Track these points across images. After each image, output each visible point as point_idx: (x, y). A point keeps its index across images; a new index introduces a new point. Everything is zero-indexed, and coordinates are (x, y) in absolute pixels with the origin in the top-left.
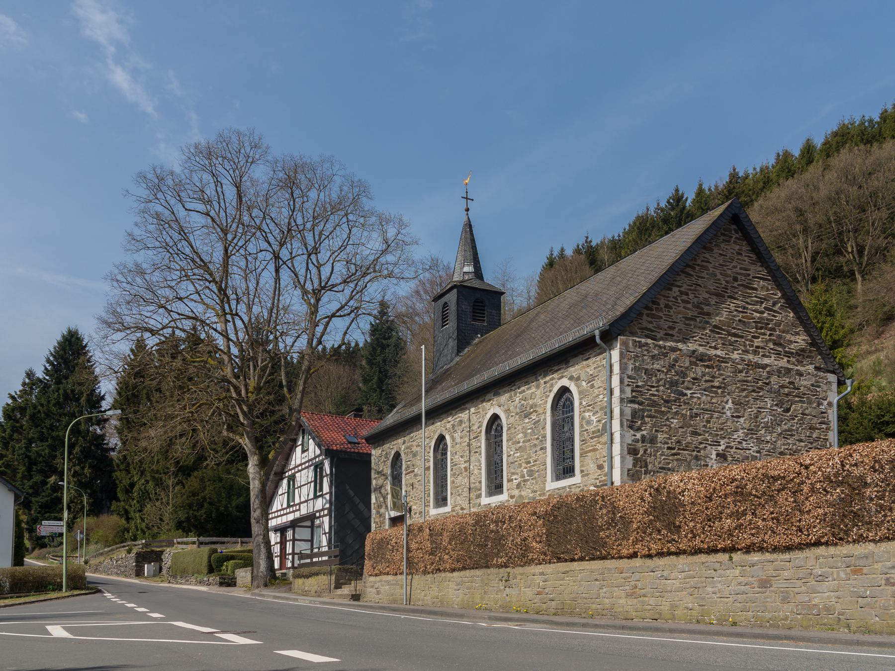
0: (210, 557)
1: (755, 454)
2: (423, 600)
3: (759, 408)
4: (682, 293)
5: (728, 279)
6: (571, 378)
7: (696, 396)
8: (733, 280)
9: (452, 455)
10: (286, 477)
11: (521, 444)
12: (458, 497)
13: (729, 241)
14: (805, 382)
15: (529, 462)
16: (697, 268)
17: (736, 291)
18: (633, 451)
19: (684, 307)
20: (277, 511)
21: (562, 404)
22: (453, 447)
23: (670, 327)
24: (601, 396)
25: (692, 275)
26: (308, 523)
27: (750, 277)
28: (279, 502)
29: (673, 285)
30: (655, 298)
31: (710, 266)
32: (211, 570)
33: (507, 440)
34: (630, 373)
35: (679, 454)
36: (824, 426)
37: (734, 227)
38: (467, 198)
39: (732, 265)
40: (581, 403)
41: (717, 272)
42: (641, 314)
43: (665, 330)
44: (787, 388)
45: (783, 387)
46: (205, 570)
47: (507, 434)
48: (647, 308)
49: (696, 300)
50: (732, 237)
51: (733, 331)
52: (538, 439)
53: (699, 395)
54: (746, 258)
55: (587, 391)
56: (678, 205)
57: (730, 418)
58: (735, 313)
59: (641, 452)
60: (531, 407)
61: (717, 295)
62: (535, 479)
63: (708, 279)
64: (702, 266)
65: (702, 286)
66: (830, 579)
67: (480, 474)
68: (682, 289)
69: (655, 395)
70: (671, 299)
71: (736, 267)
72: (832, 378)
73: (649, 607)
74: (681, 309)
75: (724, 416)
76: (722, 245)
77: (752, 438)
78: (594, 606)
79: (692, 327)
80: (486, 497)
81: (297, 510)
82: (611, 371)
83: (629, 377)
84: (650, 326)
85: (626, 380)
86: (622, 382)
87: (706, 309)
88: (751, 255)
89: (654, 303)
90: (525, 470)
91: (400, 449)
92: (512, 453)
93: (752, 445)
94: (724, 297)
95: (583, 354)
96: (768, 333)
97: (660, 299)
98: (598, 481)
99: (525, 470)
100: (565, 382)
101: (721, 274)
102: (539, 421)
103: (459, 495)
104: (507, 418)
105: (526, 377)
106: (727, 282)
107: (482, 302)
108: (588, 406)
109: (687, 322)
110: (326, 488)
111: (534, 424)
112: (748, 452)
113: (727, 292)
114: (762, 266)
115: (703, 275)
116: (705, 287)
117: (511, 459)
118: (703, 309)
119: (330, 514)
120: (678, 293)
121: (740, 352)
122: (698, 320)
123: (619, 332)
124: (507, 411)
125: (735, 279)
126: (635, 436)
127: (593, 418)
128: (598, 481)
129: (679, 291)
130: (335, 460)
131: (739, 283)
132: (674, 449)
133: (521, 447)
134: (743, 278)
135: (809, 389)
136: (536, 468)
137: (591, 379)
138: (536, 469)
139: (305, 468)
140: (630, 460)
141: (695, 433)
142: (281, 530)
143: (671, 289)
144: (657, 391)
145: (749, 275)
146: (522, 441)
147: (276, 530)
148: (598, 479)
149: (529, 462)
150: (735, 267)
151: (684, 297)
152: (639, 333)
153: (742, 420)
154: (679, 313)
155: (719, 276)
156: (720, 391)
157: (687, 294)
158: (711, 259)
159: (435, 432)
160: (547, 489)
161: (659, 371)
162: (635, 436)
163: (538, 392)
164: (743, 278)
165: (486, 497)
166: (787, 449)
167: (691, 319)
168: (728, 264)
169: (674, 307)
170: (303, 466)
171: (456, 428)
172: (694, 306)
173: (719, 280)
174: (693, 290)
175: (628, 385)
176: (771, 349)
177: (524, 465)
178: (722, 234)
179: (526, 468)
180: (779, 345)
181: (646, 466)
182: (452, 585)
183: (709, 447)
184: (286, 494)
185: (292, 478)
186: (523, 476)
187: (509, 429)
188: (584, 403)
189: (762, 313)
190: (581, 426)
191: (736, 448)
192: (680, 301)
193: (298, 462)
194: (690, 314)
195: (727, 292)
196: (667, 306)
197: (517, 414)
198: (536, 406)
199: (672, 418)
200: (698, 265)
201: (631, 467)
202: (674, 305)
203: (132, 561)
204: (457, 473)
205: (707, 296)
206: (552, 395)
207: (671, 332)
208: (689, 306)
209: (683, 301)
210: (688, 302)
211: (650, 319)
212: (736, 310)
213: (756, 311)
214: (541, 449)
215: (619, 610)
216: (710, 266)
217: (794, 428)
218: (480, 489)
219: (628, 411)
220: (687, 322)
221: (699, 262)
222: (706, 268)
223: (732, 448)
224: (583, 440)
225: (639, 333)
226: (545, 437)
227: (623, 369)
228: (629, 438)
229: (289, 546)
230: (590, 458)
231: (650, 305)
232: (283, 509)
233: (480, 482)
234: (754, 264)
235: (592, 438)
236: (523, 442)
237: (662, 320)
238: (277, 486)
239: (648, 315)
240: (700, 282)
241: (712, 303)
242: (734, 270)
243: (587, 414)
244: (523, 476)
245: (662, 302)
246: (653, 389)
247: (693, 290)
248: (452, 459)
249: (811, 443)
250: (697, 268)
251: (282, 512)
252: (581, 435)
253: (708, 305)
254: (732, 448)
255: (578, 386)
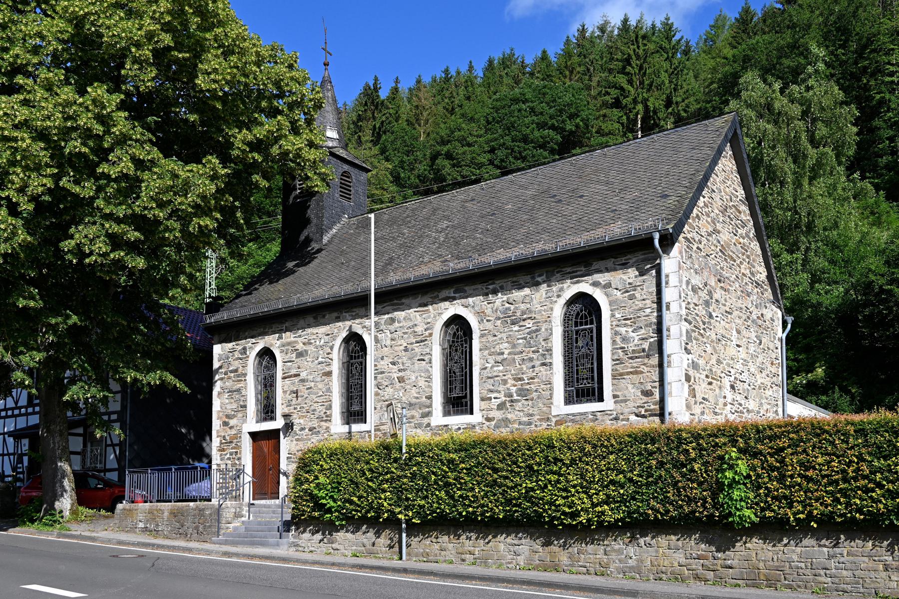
15: (521, 379)
24: (648, 311)
40: (613, 316)
56: (16, 127)
62: (532, 399)
92: (489, 365)
95: (616, 258)
104: (480, 322)
107: (349, 177)
117: (486, 373)
146: (506, 352)
148: (643, 407)
177: (511, 382)
179: (515, 386)
187: (482, 336)
188: (618, 316)
236: (509, 354)
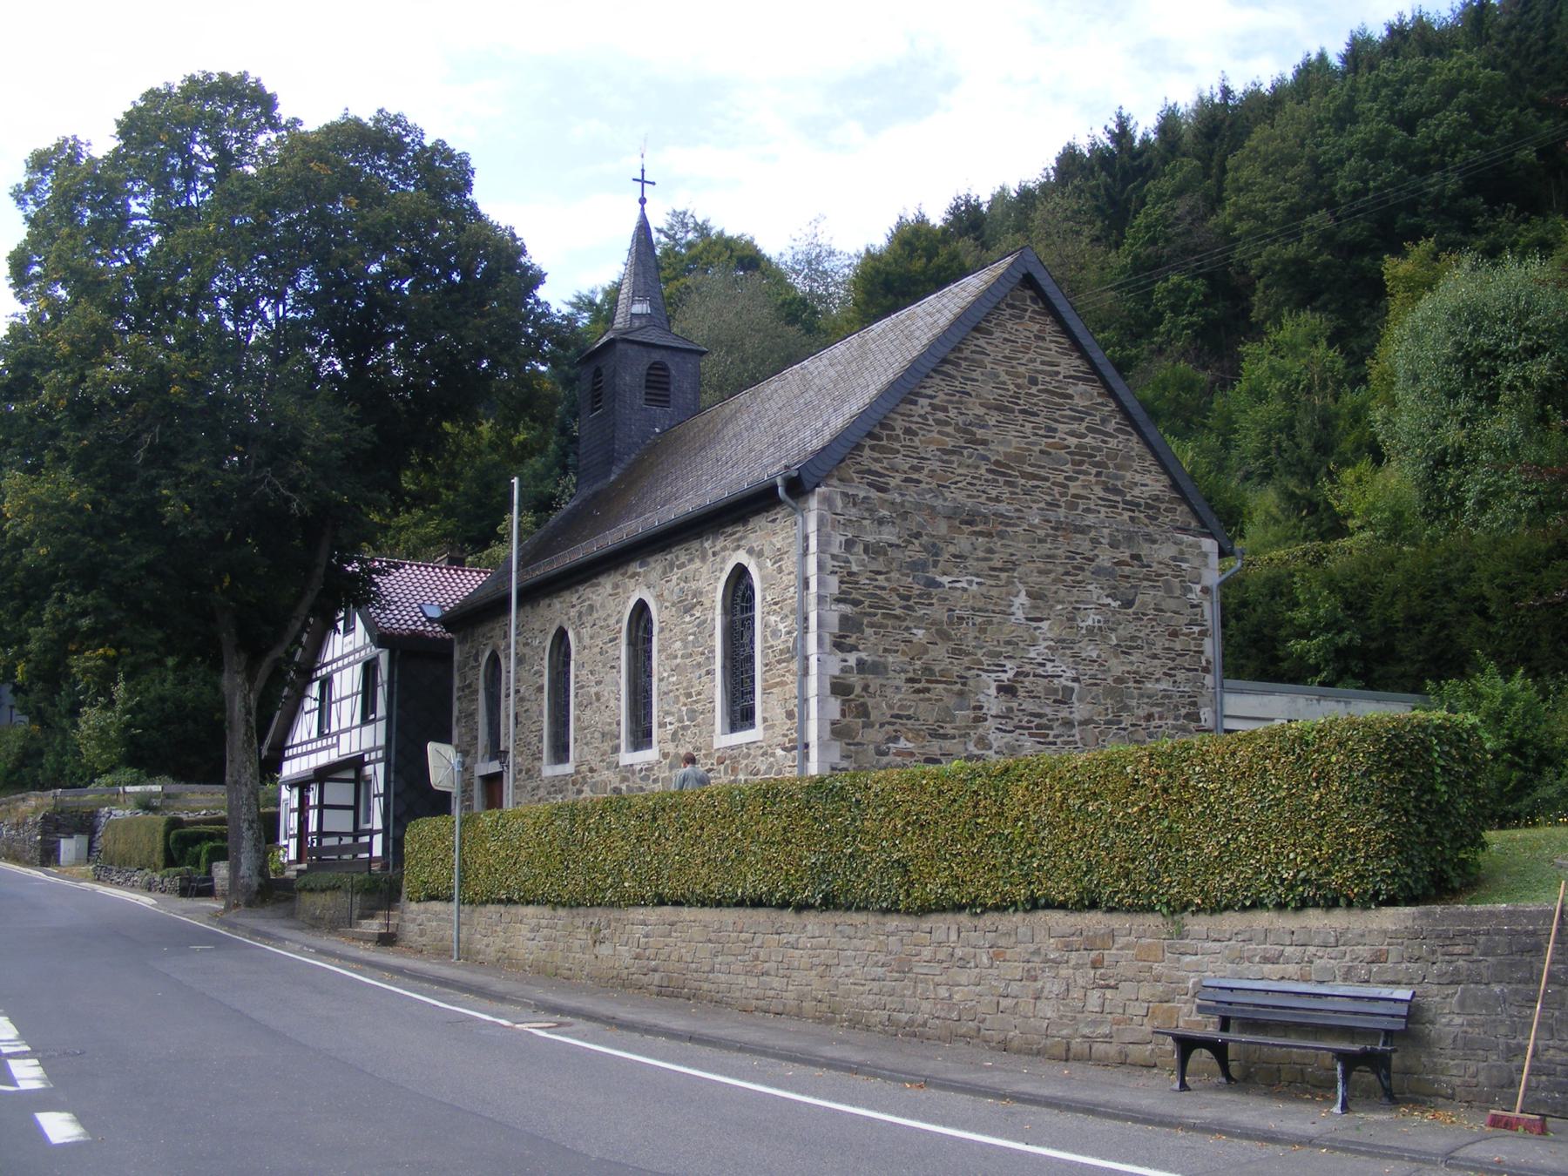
0: (167, 835)
1: (1070, 684)
2: (484, 953)
3: (1077, 602)
4: (934, 407)
5: (1019, 381)
6: (750, 552)
7: (963, 586)
8: (1030, 382)
9: (577, 669)
10: (317, 679)
11: (678, 661)
12: (586, 748)
13: (1021, 318)
14: (1166, 551)
16: (964, 364)
17: (1035, 400)
18: (839, 688)
19: (939, 432)
20: (301, 744)
21: (740, 594)
22: (578, 653)
23: (914, 468)
25: (953, 377)
26: (351, 775)
27: (1061, 377)
28: (306, 727)
29: (918, 394)
30: (885, 417)
31: (987, 360)
32: (170, 861)
33: (659, 652)
34: (836, 551)
35: (927, 690)
36: (1196, 629)
37: (1029, 293)
38: (643, 181)
39: (1027, 356)
40: (764, 599)
41: (1000, 369)
42: (859, 447)
43: (905, 472)
44: (1128, 565)
45: (1120, 563)
46: (158, 858)
47: (659, 639)
48: (871, 435)
49: (961, 419)
50: (1026, 310)
51: (1030, 470)
52: (702, 654)
53: (965, 585)
54: (1052, 346)
55: (773, 577)
57: (1023, 621)
58: (1033, 438)
59: (858, 690)
60: (694, 596)
61: (1000, 409)
63: (983, 381)
64: (973, 360)
65: (974, 394)
66: (972, 964)
67: (619, 707)
68: (935, 401)
69: (884, 588)
70: (916, 419)
71: (1034, 361)
72: (1209, 545)
73: (772, 993)
74: (935, 435)
75: (1013, 618)
76: (1009, 325)
77: (1064, 655)
78: (706, 986)
79: (955, 466)
80: (627, 751)
81: (333, 746)
82: (806, 549)
83: (834, 557)
84: (876, 467)
85: (830, 563)
86: (820, 567)
87: (980, 433)
88: (1062, 340)
89: (883, 426)
90: (684, 709)
91: (499, 647)
92: (665, 675)
93: (1064, 668)
94: (1013, 411)
96: (1094, 471)
97: (895, 420)
98: (787, 740)
99: (684, 709)
100: (741, 557)
101: (1007, 373)
102: (705, 621)
103: (587, 744)
104: (660, 612)
105: (686, 540)
106: (1018, 386)
108: (776, 604)
109: (945, 457)
110: (381, 710)
111: (698, 626)
112: (1056, 681)
113: (1018, 404)
114: (1079, 358)
115: (974, 375)
116: (978, 396)
118: (974, 434)
119: (387, 760)
120: (929, 409)
121: (1042, 505)
122: (965, 452)
123: (816, 480)
124: (659, 597)
125: (1033, 381)
126: (845, 661)
127: (781, 626)
128: (787, 740)
129: (930, 404)
130: (398, 653)
131: (1040, 387)
132: (918, 681)
133: (678, 665)
134: (1048, 379)
135: (1168, 565)
136: (698, 707)
137: (779, 557)
138: (701, 709)
139: (350, 664)
140: (835, 705)
141: (957, 652)
142: (302, 784)
143: (915, 403)
144: (888, 580)
145: (1058, 373)
146: (680, 653)
147: (292, 784)
149: (689, 695)
150: (1032, 361)
151: (940, 415)
152: (857, 480)
153: (1045, 625)
154: (930, 443)
155: (1004, 377)
156: (1004, 575)
157: (945, 410)
158: (989, 349)
159: (551, 621)
160: (715, 747)
161: (891, 545)
162: (845, 661)
163: (704, 569)
164: (1048, 379)
165: (627, 751)
166: (1128, 672)
167: (952, 452)
168: (1020, 355)
169: (921, 432)
170: (346, 661)
171: (584, 619)
172: (958, 429)
173: (1004, 383)
174: (957, 402)
175: (833, 573)
176: (1100, 498)
177: (683, 699)
178: (1009, 306)
179: (685, 705)
180: (1116, 491)
181: (866, 714)
182: (524, 930)
183: (984, 675)
184: (317, 712)
185: (326, 683)
186: (681, 720)
187: (662, 630)
188: (769, 598)
189: (1082, 436)
190: (765, 639)
191: (1035, 676)
192: (931, 422)
193: (338, 654)
194: (950, 443)
195: (1018, 404)
196: (908, 431)
197: (673, 605)
198: (701, 593)
199: (916, 627)
200: (965, 359)
201: (837, 716)
202: (921, 429)
203: (36, 831)
204: (585, 702)
205: (981, 411)
206: (724, 577)
207: (915, 476)
208: (949, 430)
209: (938, 422)
210: (947, 424)
211: (876, 455)
212: (1037, 435)
213: (1072, 434)
214: (708, 673)
215: (738, 994)
216: (987, 360)
217: (1142, 635)
218: (618, 737)
219: (833, 619)
220: (945, 457)
221: (967, 353)
222: (982, 365)
223: (1027, 675)
224: (767, 665)
225: (857, 480)
226: (713, 651)
227: (823, 546)
228: (834, 667)
229: (313, 816)
230: (775, 696)
231: (877, 430)
232: (311, 741)
233: (618, 724)
234: (1066, 354)
235: (779, 662)
237: (900, 456)
238: (301, 696)
239: (872, 448)
240: (968, 388)
241: (990, 423)
242: (1031, 366)
243: (773, 618)
244: (681, 720)
245: (899, 424)
246: (879, 577)
247: (957, 402)
248: (577, 676)
249: (1173, 660)
250: (964, 364)
251: (310, 747)
252: (765, 655)
253: (983, 427)
254: (1027, 675)
255: (761, 567)
